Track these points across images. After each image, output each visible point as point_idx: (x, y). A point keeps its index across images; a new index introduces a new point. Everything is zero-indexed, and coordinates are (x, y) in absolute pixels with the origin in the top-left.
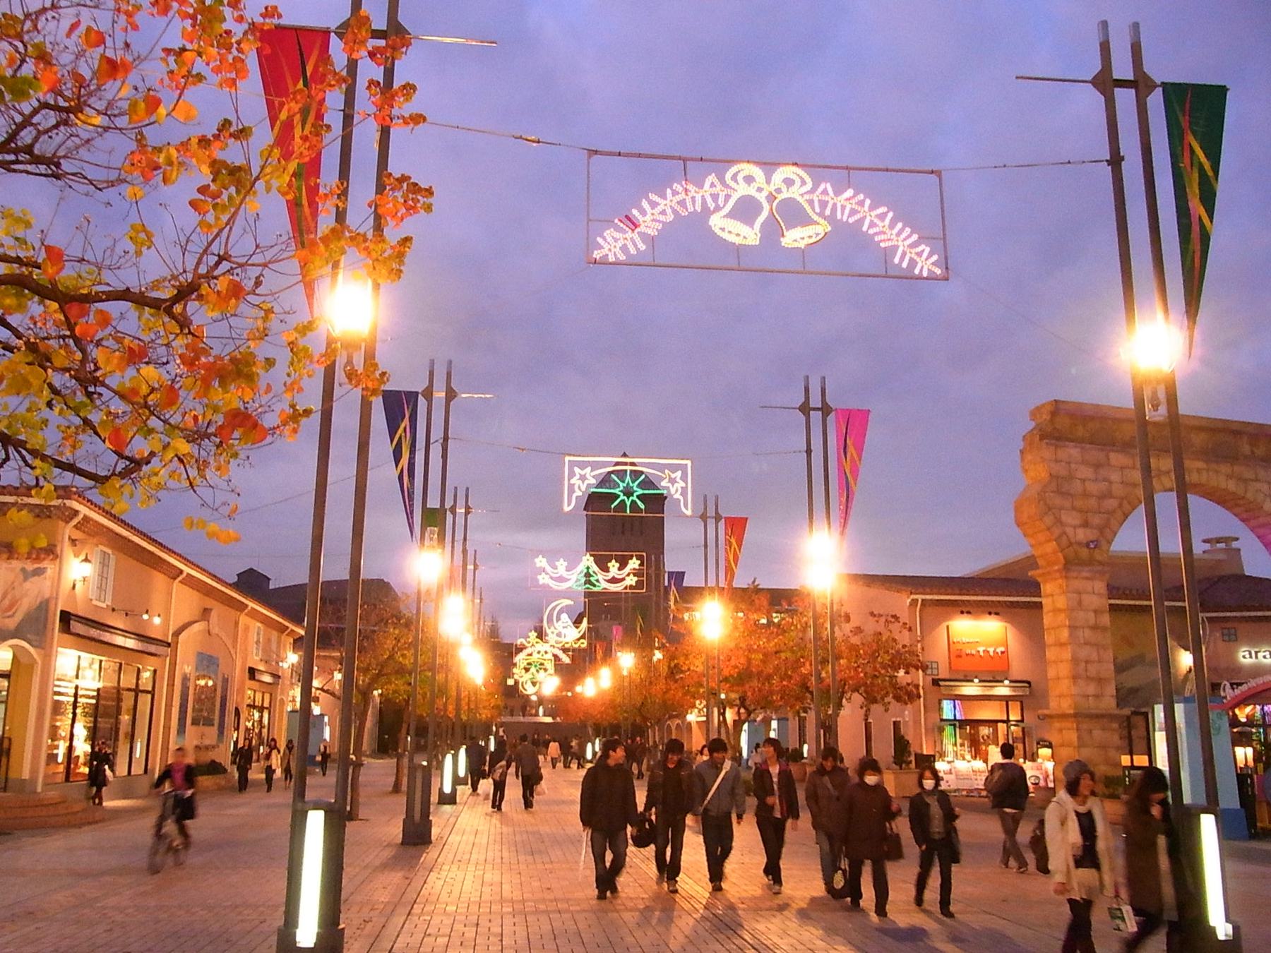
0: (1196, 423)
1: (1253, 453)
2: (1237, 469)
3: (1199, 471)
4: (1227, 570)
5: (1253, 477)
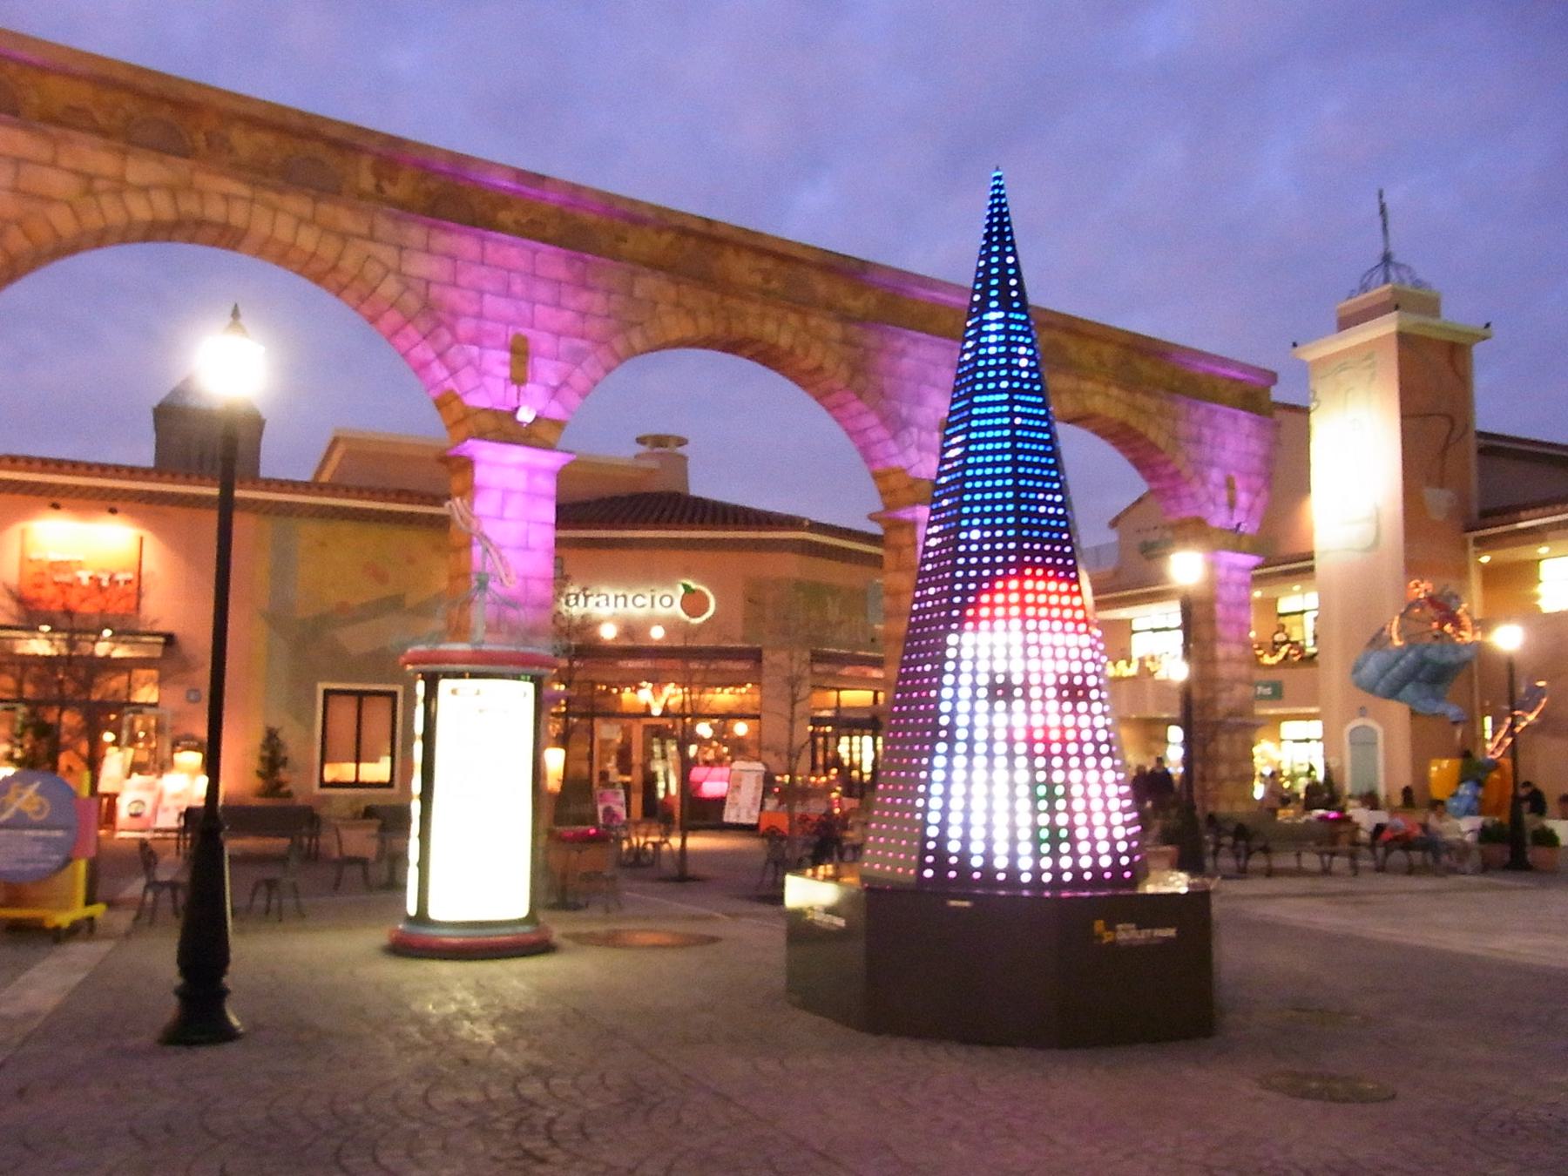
0: (242, 108)
1: (379, 188)
2: (326, 210)
3: (227, 198)
4: (657, 486)
5: (364, 230)
